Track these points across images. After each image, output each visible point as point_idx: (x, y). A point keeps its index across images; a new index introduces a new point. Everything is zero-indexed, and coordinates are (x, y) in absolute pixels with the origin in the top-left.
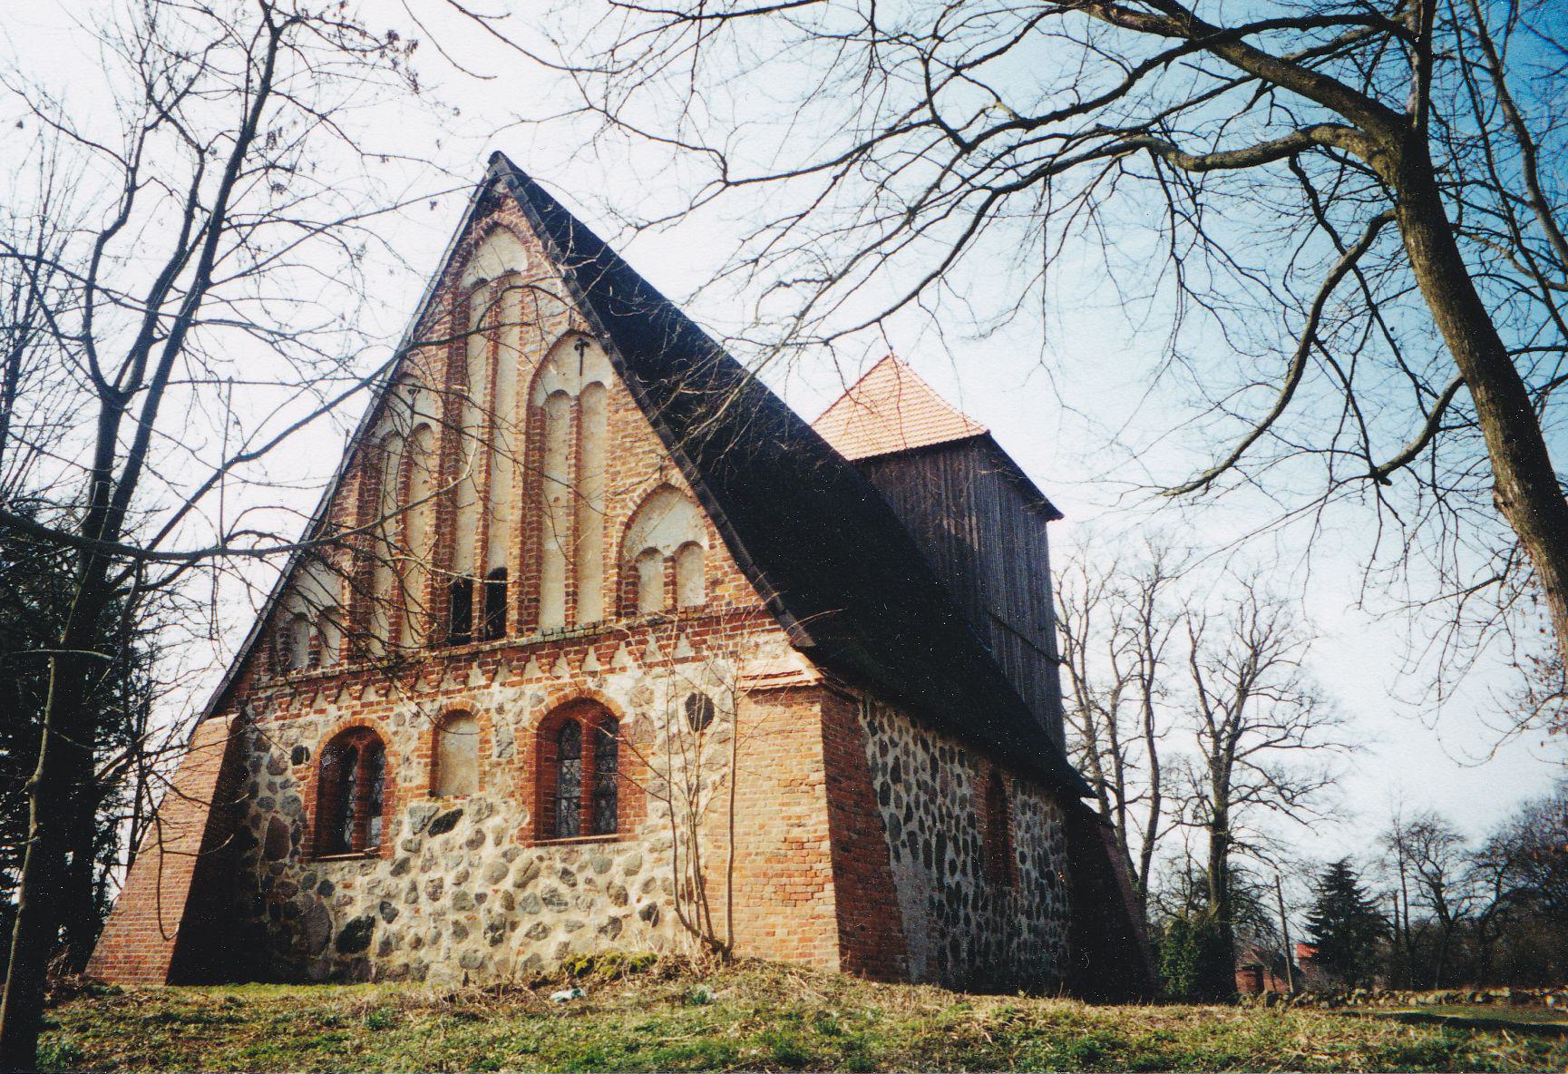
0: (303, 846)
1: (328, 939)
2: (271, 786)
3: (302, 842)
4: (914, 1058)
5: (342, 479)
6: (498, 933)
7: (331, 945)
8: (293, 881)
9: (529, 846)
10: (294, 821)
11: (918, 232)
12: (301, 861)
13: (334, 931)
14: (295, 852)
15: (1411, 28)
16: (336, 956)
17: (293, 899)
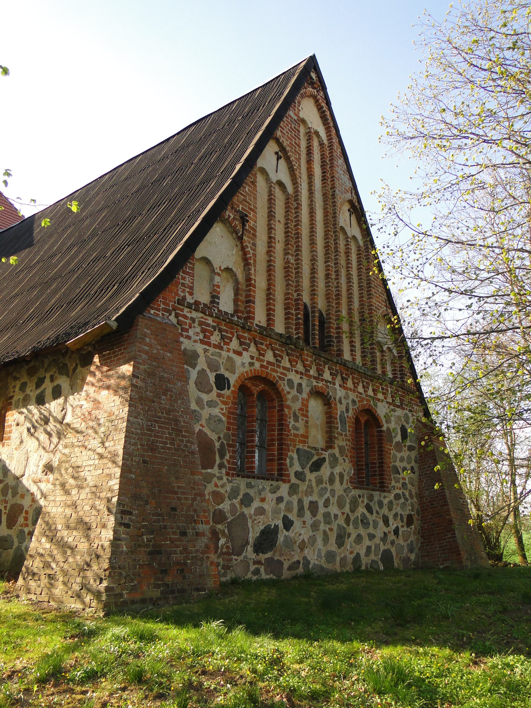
0: (228, 462)
1: (247, 543)
2: (199, 401)
3: (227, 457)
4: (513, 135)
5: (261, 87)
6: (340, 541)
7: (250, 548)
8: (222, 491)
9: (354, 488)
10: (219, 438)
11: (517, 35)
12: (227, 474)
13: (251, 535)
14: (221, 466)
15: (516, 463)
16: (253, 556)
17: (221, 507)
